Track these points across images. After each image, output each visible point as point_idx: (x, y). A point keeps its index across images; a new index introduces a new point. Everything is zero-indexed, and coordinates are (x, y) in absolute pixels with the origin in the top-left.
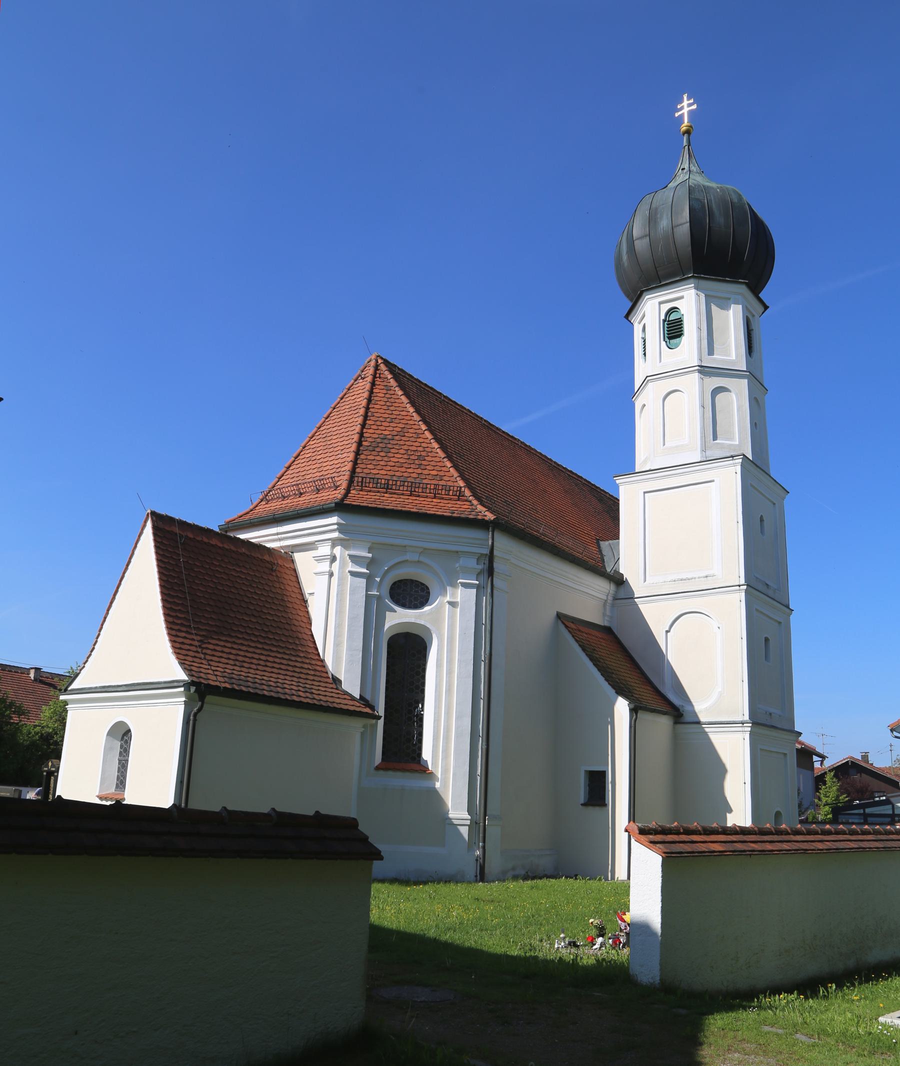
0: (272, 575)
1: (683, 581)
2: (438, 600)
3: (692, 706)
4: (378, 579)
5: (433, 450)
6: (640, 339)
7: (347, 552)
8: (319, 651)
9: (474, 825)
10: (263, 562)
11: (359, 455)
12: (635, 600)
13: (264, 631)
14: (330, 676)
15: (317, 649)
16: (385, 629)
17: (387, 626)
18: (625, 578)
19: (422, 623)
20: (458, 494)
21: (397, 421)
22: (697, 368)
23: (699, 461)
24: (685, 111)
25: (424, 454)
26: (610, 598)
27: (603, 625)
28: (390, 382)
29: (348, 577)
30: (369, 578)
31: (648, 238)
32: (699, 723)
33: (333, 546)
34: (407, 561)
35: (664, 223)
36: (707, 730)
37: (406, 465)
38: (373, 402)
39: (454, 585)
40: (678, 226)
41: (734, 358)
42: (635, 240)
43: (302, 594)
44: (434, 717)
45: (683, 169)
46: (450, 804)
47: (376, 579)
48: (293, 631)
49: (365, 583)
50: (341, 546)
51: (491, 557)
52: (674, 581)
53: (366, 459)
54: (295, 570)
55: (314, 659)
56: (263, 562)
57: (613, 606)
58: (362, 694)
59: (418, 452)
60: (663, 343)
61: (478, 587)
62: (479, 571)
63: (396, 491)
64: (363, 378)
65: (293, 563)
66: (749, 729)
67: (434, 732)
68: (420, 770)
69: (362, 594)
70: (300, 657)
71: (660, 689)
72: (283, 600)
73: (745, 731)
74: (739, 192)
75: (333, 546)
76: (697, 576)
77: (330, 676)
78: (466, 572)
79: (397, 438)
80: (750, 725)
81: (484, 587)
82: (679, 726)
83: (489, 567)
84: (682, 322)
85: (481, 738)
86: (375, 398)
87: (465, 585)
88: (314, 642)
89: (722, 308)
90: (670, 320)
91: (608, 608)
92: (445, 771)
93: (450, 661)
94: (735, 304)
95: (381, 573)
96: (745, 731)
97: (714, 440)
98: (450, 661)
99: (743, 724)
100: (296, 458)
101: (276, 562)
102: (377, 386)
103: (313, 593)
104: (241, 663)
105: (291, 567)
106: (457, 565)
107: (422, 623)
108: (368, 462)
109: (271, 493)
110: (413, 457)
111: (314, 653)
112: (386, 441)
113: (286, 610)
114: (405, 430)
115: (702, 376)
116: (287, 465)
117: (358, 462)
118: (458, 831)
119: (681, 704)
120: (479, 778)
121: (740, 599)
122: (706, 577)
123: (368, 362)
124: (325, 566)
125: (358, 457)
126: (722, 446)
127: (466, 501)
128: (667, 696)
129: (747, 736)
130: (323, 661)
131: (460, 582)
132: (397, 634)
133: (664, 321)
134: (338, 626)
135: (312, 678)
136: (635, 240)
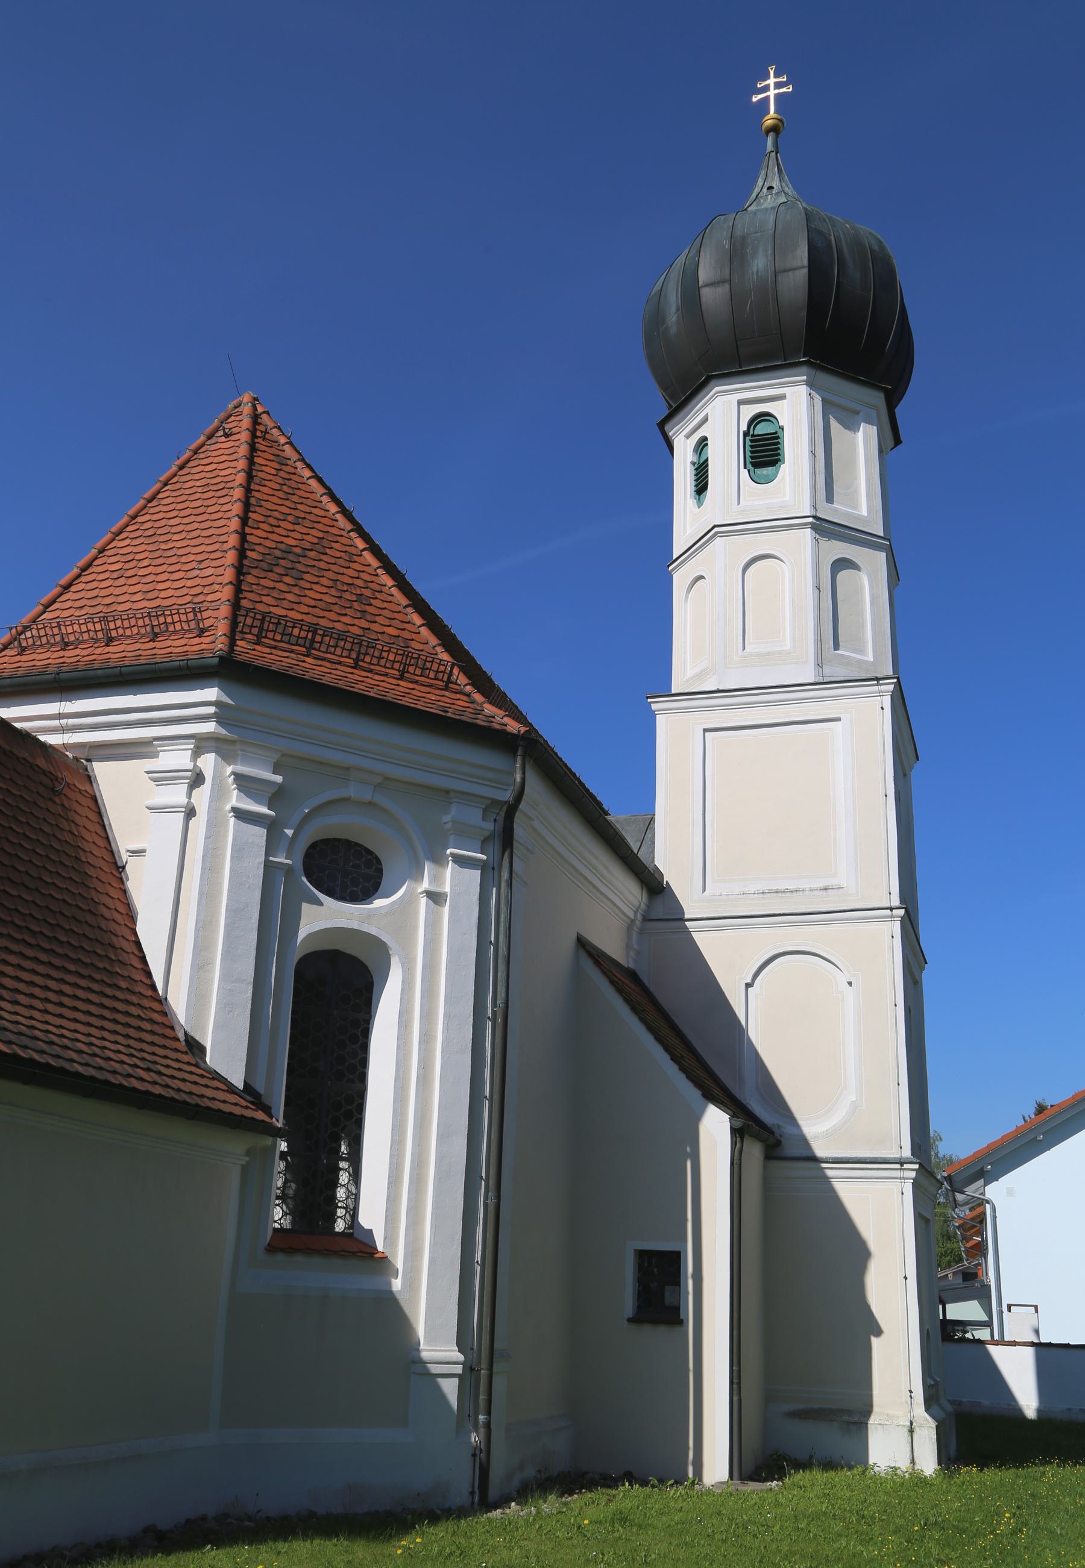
0: (55, 803)
1: (780, 895)
2: (406, 884)
3: (797, 1126)
4: (289, 832)
5: (383, 589)
6: (689, 465)
7: (229, 769)
8: (155, 978)
9: (469, 1376)
10: (33, 769)
11: (244, 574)
12: (687, 923)
13: (48, 923)
14: (181, 1036)
15: (149, 974)
16: (299, 941)
17: (302, 934)
18: (665, 883)
19: (374, 931)
20: (445, 679)
21: (307, 523)
22: (810, 520)
23: (812, 680)
24: (772, 93)
25: (367, 593)
26: (639, 917)
27: (626, 966)
28: (284, 451)
29: (228, 821)
30: (273, 827)
31: (727, 286)
32: (814, 1159)
33: (197, 753)
34: (346, 800)
35: (760, 263)
36: (829, 1173)
37: (336, 608)
38: (256, 480)
39: (439, 860)
40: (785, 271)
41: (864, 513)
42: (703, 287)
43: (112, 852)
44: (392, 1136)
45: (770, 188)
46: (421, 1330)
47: (286, 831)
48: (102, 929)
49: (265, 838)
50: (217, 752)
51: (511, 809)
52: (763, 893)
53: (258, 584)
54: (94, 799)
55: (146, 997)
56: (33, 769)
57: (642, 932)
58: (249, 1082)
59: (355, 588)
60: (744, 473)
61: (483, 867)
62: (488, 834)
63: (328, 656)
64: (226, 435)
65: (91, 783)
66: (913, 1174)
67: (390, 1168)
68: (343, 1251)
69: (258, 860)
70: (120, 988)
71: (733, 1092)
72: (78, 859)
73: (904, 1179)
74: (879, 236)
75: (197, 753)
76: (806, 886)
77: (181, 1036)
78: (463, 835)
79: (312, 554)
80: (916, 1166)
81: (493, 868)
82: (775, 1164)
83: (504, 829)
84: (780, 440)
85: (483, 1183)
86: (260, 474)
87: (460, 861)
88: (143, 959)
89: (847, 427)
90: (756, 433)
91: (635, 935)
92: (413, 1253)
93: (428, 1016)
94: (866, 423)
95: (297, 818)
96: (904, 1179)
97: (834, 650)
98: (428, 1016)
99: (902, 1164)
100: (84, 569)
101: (60, 775)
102: (260, 453)
103: (144, 851)
104: (12, 994)
105: (88, 791)
106: (447, 818)
107: (374, 933)
108: (262, 590)
109: (28, 634)
110: (347, 595)
111: (144, 983)
112: (291, 557)
113: (85, 882)
114: (325, 543)
115: (817, 536)
116: (64, 581)
117: (243, 588)
118: (438, 1389)
119: (776, 1122)
120: (478, 1269)
121: (892, 934)
122: (826, 889)
123: (236, 407)
124: (177, 794)
125: (242, 578)
126: (847, 662)
127: (460, 692)
128: (749, 1107)
129: (908, 1188)
130: (162, 1001)
131: (452, 854)
132: (316, 951)
133: (746, 434)
134: (204, 926)
135: (148, 1038)
136: (703, 287)
